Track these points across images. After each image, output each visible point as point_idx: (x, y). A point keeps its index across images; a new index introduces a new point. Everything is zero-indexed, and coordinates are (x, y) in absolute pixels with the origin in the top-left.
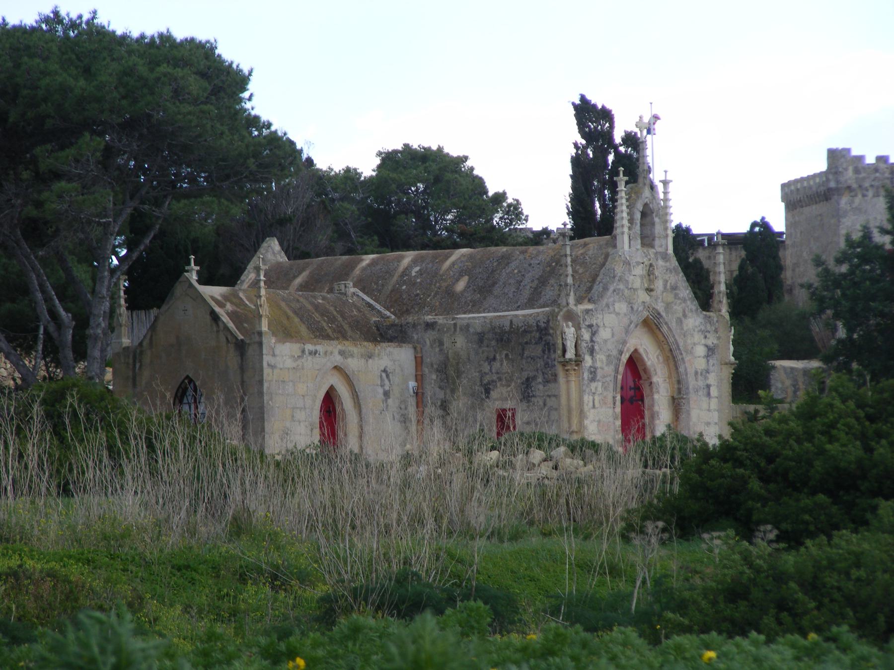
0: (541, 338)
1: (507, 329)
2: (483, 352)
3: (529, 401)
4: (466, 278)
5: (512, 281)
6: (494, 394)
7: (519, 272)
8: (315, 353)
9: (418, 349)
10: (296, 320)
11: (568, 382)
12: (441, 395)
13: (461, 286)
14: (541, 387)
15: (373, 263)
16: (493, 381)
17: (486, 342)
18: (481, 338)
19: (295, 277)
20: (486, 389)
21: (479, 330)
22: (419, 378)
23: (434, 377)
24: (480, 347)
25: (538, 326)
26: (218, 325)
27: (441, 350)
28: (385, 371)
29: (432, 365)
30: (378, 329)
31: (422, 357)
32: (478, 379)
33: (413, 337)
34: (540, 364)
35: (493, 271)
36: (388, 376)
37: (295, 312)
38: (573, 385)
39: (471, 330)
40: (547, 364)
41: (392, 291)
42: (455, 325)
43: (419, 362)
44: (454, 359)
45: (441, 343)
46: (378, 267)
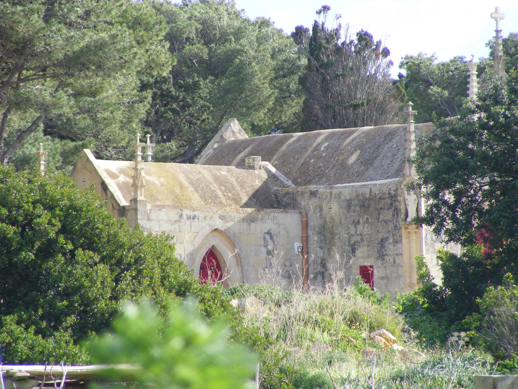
0: (392, 204)
1: (368, 196)
2: (350, 217)
3: (383, 259)
4: (359, 152)
5: (390, 154)
6: (358, 253)
7: (397, 146)
8: (194, 218)
9: (304, 214)
10: (191, 189)
11: (409, 243)
12: (321, 254)
13: (353, 159)
14: (391, 247)
15: (299, 139)
16: (357, 242)
17: (352, 208)
18: (349, 204)
19: (240, 152)
20: (352, 249)
21: (348, 198)
22: (305, 240)
23: (316, 238)
24: (348, 212)
25: (389, 193)
26: (106, 194)
27: (321, 215)
28: (268, 233)
29: (315, 229)
30: (276, 197)
31: (307, 221)
32: (347, 240)
33: (301, 204)
34: (391, 226)
35: (379, 146)
36: (271, 238)
37: (192, 183)
38: (414, 244)
39: (343, 198)
40: (396, 226)
41: (303, 164)
42: (331, 193)
43: (305, 226)
44: (330, 223)
45: (321, 209)
46: (300, 143)
